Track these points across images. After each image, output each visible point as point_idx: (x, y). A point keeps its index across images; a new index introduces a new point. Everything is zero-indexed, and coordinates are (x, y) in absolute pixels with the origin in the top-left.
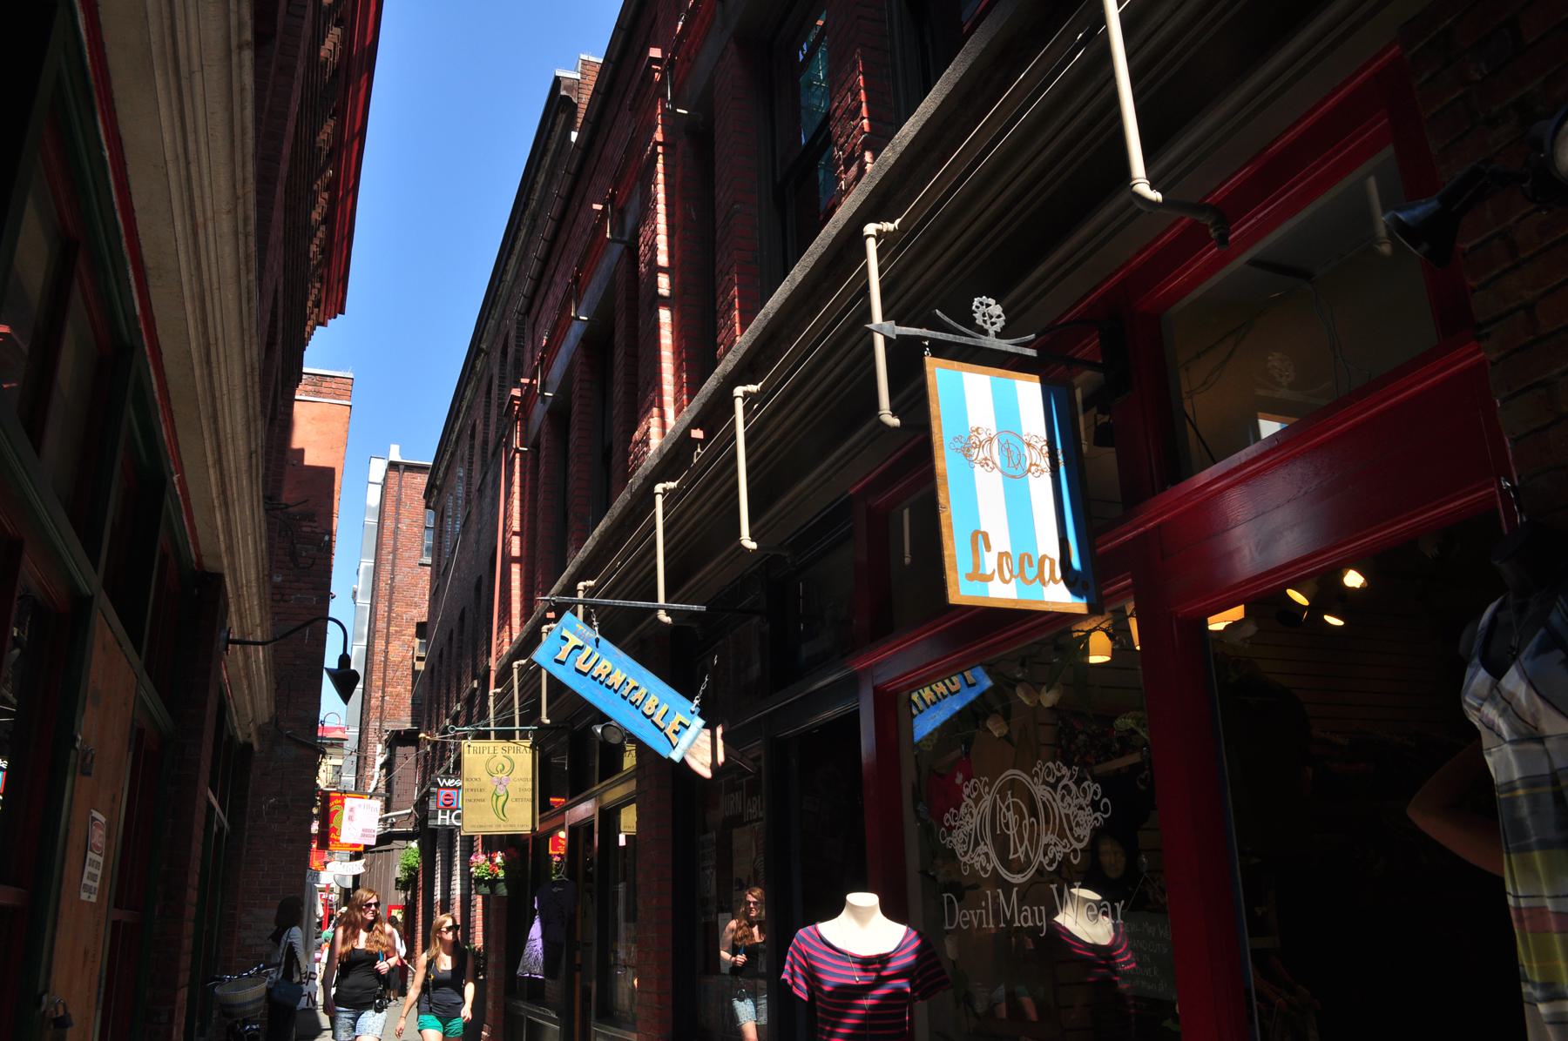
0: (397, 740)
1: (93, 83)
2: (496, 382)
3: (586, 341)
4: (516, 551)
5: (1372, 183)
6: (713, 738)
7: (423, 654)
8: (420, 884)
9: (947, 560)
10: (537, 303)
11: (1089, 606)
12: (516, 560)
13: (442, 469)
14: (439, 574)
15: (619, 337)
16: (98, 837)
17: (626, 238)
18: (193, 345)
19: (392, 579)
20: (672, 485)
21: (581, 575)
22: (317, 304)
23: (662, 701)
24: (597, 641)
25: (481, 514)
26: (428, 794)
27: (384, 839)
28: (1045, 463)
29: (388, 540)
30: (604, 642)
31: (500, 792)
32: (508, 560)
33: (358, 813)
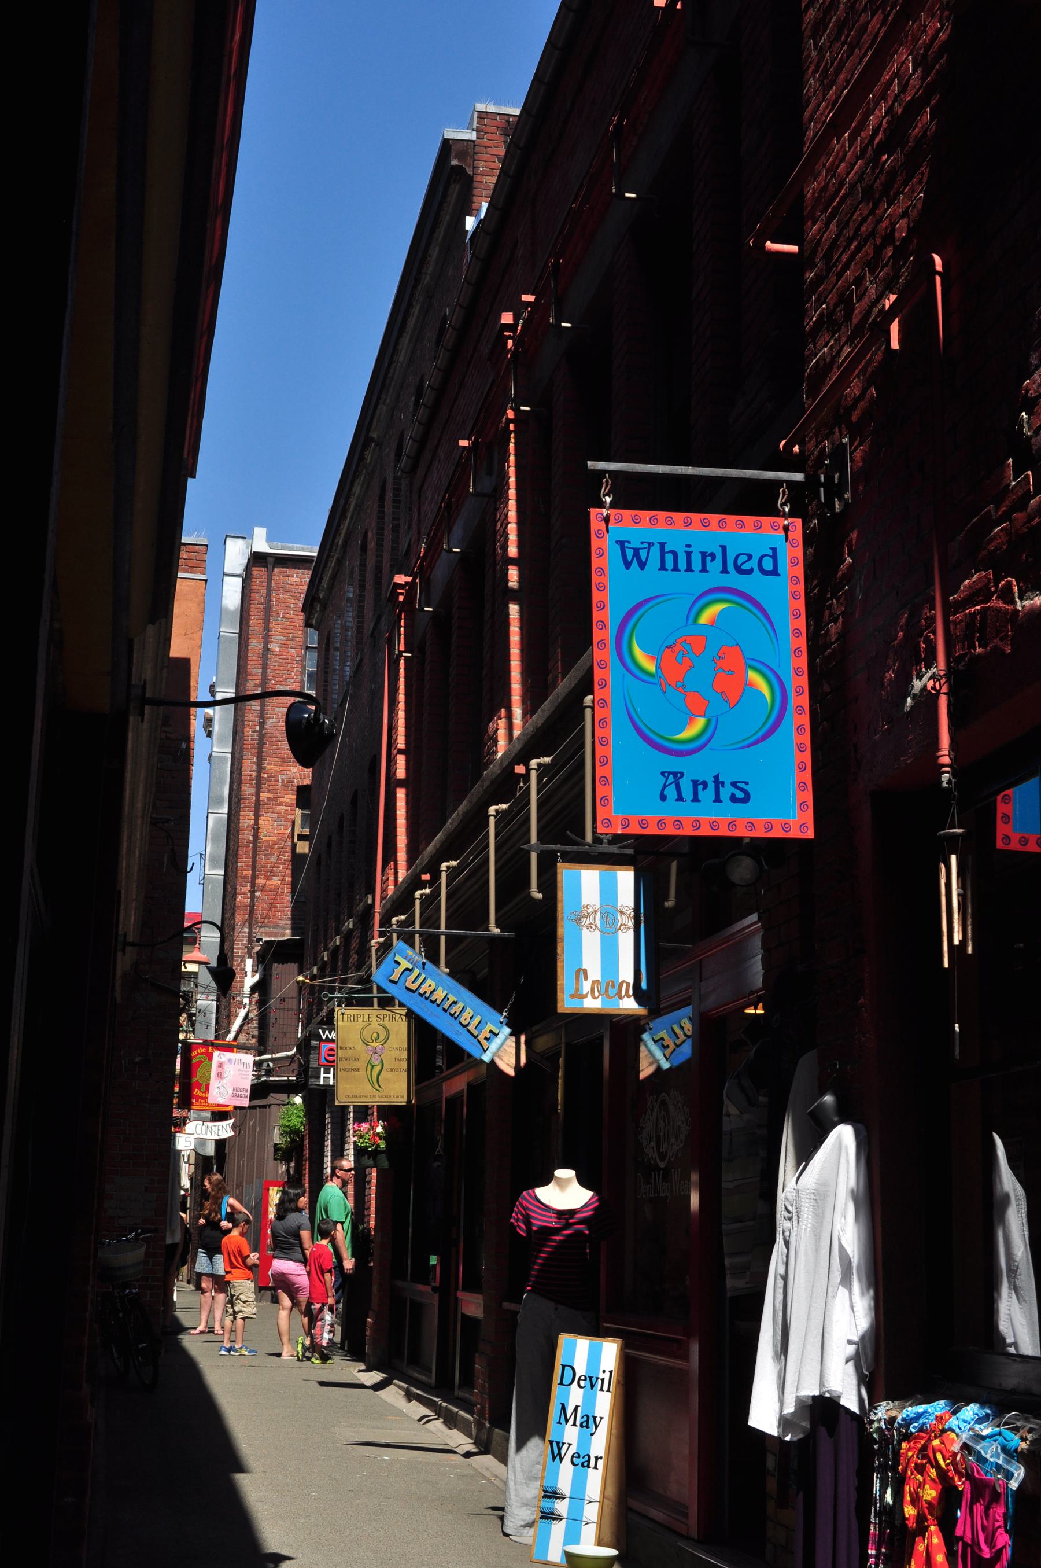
0: (271, 955)
4: (401, 773)
7: (307, 831)
12: (401, 783)
19: (262, 725)
23: (476, 1013)
24: (424, 964)
27: (259, 1091)
28: (631, 923)
31: (375, 1061)
32: (393, 783)
33: (230, 1070)
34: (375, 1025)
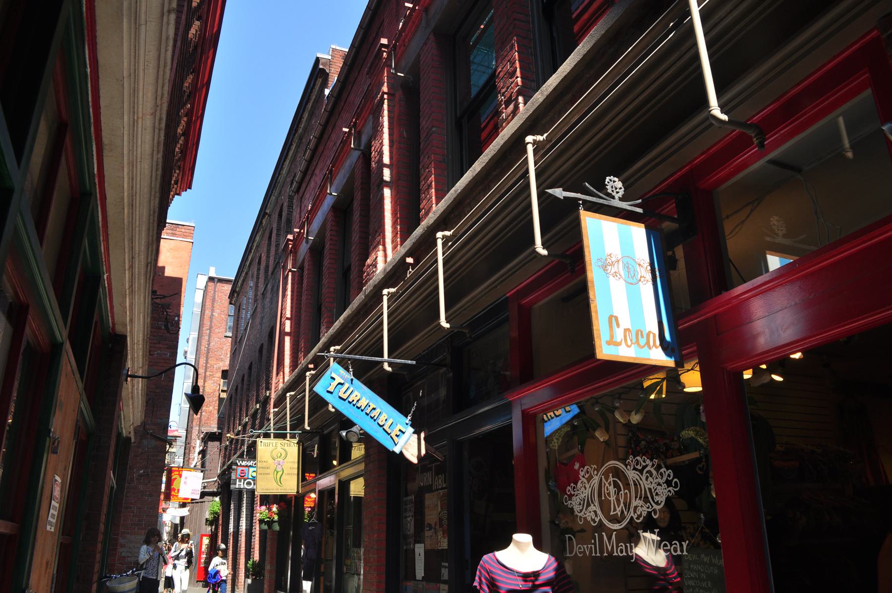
0: (210, 437)
1: (85, 24)
2: (275, 232)
3: (335, 208)
4: (288, 329)
5: (841, 120)
6: (419, 439)
7: (225, 389)
8: (220, 522)
9: (595, 332)
10: (304, 185)
11: (676, 362)
13: (240, 282)
14: (237, 342)
15: (356, 204)
16: (57, 492)
17: (362, 148)
18: (126, 194)
19: (209, 345)
20: (392, 290)
21: (332, 341)
22: (176, 183)
24: (352, 380)
25: (263, 307)
26: (230, 468)
28: (649, 276)
29: (207, 323)
30: (355, 381)
31: (278, 470)
32: (283, 334)
34: (279, 449)
